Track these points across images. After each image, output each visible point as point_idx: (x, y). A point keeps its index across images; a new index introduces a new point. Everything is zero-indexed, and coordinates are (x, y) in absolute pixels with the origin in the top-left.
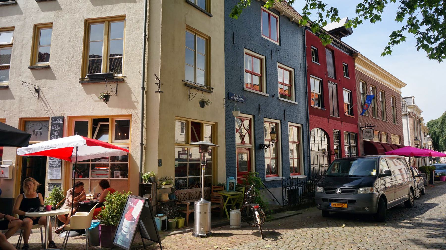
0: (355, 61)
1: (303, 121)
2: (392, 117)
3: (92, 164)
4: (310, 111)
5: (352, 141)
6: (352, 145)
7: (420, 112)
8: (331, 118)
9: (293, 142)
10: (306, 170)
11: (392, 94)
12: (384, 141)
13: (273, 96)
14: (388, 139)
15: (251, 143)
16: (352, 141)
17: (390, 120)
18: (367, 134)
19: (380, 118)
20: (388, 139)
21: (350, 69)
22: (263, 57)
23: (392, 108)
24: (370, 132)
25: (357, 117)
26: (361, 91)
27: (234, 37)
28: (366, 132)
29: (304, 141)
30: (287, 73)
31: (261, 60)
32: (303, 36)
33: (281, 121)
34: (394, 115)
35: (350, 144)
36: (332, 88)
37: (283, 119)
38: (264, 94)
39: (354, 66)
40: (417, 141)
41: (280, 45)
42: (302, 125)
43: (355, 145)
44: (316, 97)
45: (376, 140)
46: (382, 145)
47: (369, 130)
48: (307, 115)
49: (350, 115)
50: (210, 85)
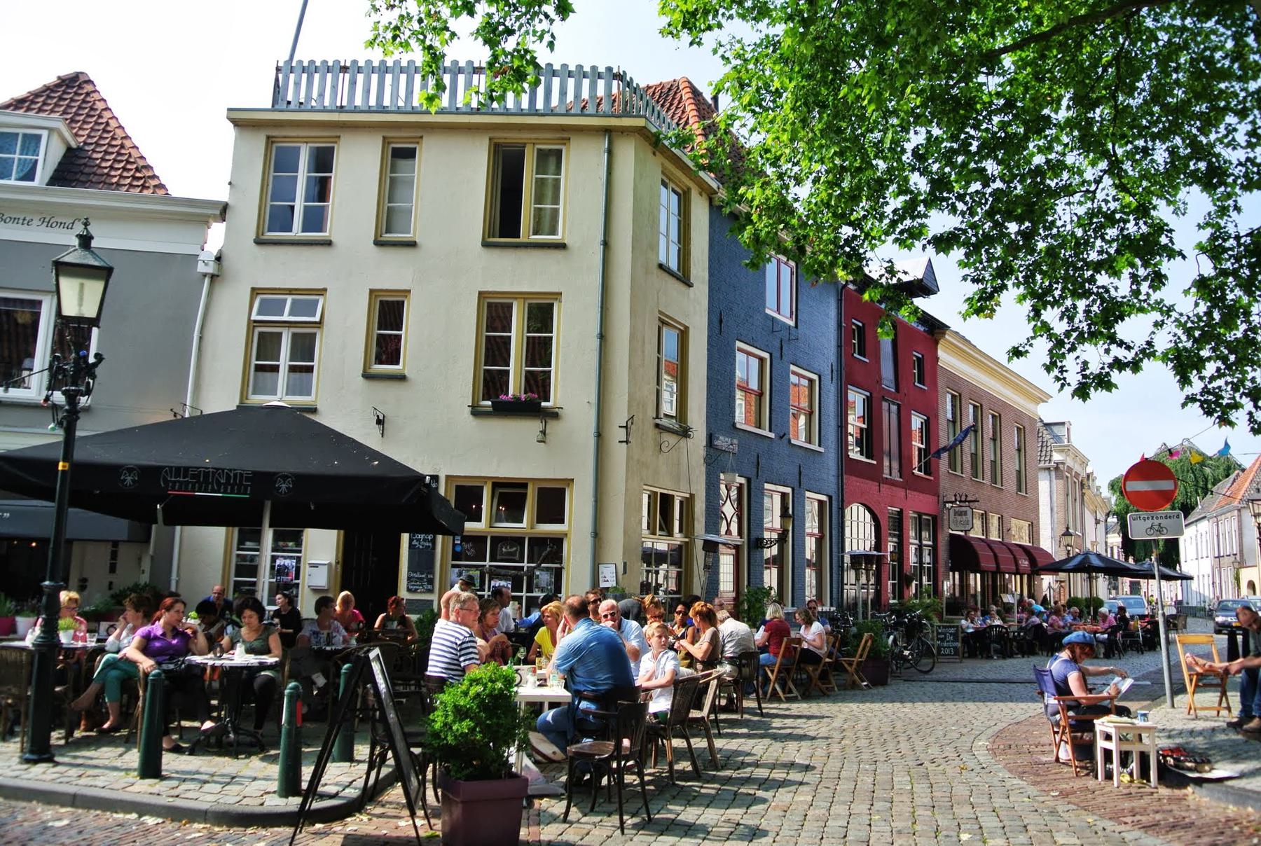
0: (939, 346)
1: (832, 489)
2: (1014, 475)
3: (491, 561)
4: (846, 466)
5: (925, 534)
6: (924, 542)
7: (1084, 462)
8: (887, 481)
9: (811, 535)
10: (835, 596)
11: (951, 386)
12: (994, 536)
13: (781, 437)
14: (1003, 529)
15: (740, 533)
16: (925, 534)
17: (1010, 484)
18: (959, 518)
19: (987, 481)
20: (1003, 529)
21: (927, 367)
22: (766, 355)
23: (1016, 454)
24: (966, 513)
25: (937, 478)
26: (950, 416)
27: (721, 321)
28: (956, 513)
29: (834, 532)
30: (754, 363)
31: (761, 360)
32: (839, 301)
33: (793, 490)
34: (1019, 472)
35: (920, 540)
36: (889, 413)
37: (797, 484)
38: (766, 433)
39: (937, 359)
40: (1069, 538)
41: (796, 326)
42: (830, 498)
43: (931, 543)
44: (856, 434)
45: (976, 533)
46: (989, 544)
47: (964, 509)
48: (840, 476)
49: (922, 474)
50: (685, 422)
